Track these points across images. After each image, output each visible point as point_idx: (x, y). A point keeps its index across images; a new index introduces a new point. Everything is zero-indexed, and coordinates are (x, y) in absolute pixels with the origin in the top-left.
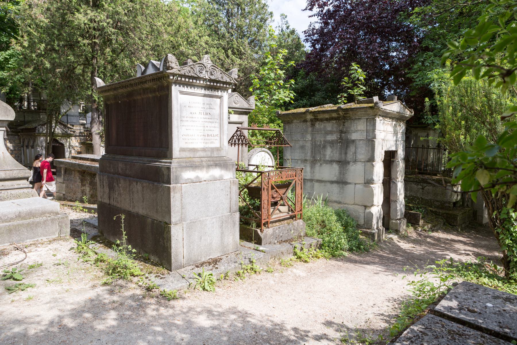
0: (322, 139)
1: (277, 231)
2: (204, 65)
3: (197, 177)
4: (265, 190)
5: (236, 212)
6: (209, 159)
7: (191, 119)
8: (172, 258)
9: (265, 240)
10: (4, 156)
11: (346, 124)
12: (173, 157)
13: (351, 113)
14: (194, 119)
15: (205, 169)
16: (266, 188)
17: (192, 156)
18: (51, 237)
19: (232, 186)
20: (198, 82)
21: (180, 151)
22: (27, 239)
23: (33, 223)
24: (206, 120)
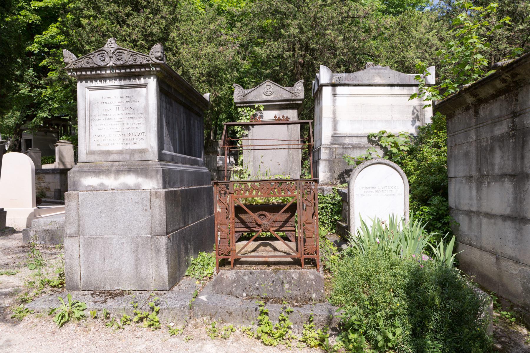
0: (489, 135)
1: (246, 278)
2: (105, 51)
3: (102, 184)
5: (161, 235)
11: (520, 98)
12: (79, 161)
13: (520, 70)
15: (112, 176)
17: (103, 160)
19: (153, 199)
20: (103, 72)
24: (125, 116)
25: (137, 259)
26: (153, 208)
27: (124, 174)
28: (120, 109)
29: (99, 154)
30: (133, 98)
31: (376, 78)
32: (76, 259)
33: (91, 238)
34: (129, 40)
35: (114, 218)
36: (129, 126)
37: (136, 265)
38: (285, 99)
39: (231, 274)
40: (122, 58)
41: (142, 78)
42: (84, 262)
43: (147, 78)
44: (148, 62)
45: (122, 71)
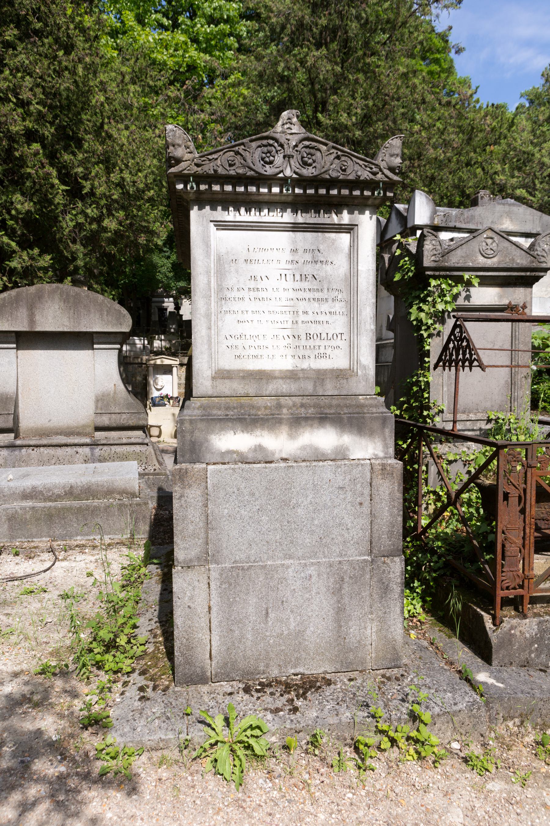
2: (276, 140)
3: (260, 448)
4: (514, 501)
5: (391, 554)
6: (305, 400)
7: (253, 294)
8: (176, 654)
9: (502, 652)
10: (115, 390)
12: (194, 395)
14: (261, 294)
15: (284, 430)
16: (514, 493)
17: (251, 391)
18: (116, 536)
19: (378, 481)
20: (264, 190)
21: (213, 378)
22: (77, 535)
23: (88, 508)
24: (301, 295)
25: (339, 607)
26: (376, 499)
27: (311, 426)
28: (290, 278)
29: (243, 378)
30: (319, 254)
31: (504, 221)
32: (201, 616)
33: (238, 568)
34: (15, 100)
35: (288, 522)
36: (310, 317)
37: (338, 621)
38: (520, 266)
39: (530, 627)
40: (314, 162)
41: (345, 212)
42: (221, 622)
43: (356, 212)
44: (373, 177)
45: (308, 191)
